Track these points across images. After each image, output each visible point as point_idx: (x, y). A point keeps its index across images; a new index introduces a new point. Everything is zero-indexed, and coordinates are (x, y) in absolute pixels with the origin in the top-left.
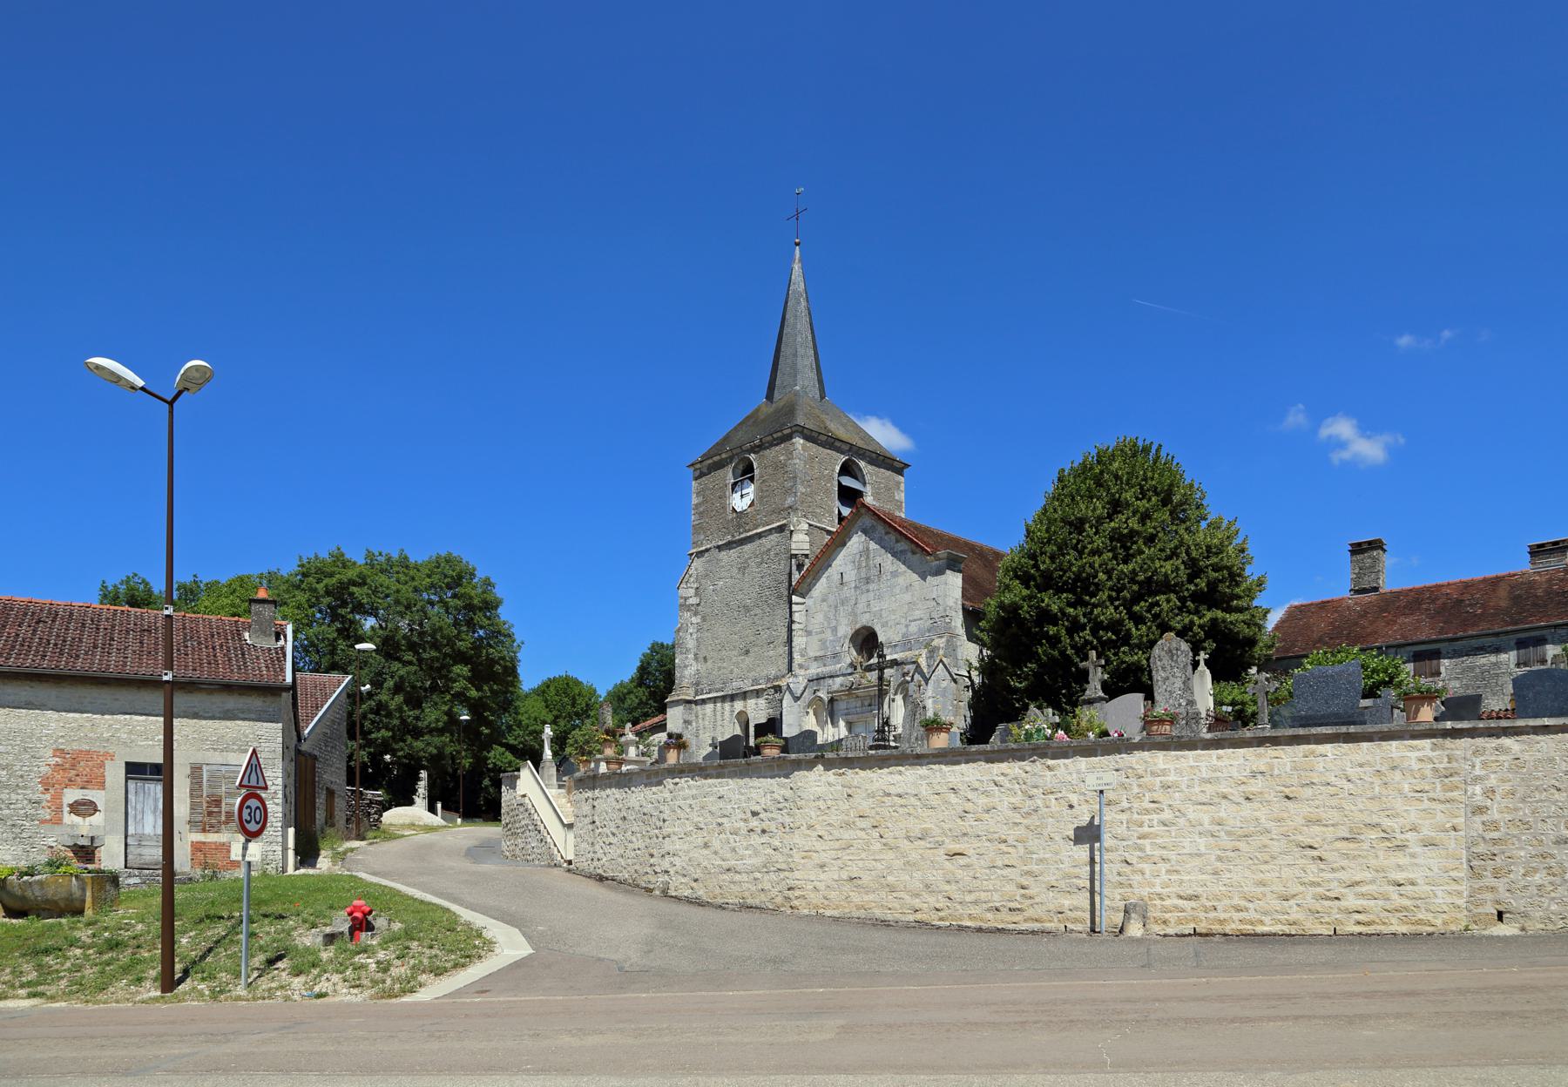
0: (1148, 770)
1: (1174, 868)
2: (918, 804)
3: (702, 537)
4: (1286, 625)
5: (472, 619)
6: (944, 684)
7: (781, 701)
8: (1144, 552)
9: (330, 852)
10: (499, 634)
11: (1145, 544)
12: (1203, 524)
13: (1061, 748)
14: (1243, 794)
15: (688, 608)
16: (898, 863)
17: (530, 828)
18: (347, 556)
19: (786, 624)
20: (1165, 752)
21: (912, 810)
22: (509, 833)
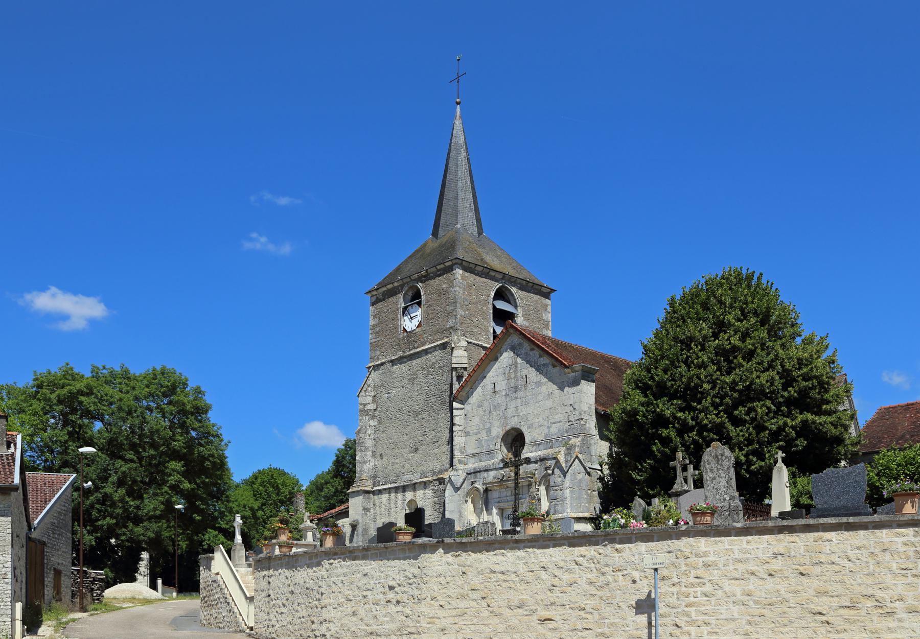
0: (693, 552)
1: (714, 630)
2: (517, 579)
3: (378, 353)
4: (875, 424)
5: (185, 422)
6: (580, 476)
7: (444, 491)
8: (743, 366)
9: (54, 623)
10: (209, 435)
11: (744, 359)
12: (798, 340)
13: (626, 534)
14: (766, 571)
15: (367, 413)
16: (502, 627)
17: (221, 600)
18: (76, 370)
19: (449, 426)
20: (706, 538)
21: (512, 585)
22: (206, 605)
